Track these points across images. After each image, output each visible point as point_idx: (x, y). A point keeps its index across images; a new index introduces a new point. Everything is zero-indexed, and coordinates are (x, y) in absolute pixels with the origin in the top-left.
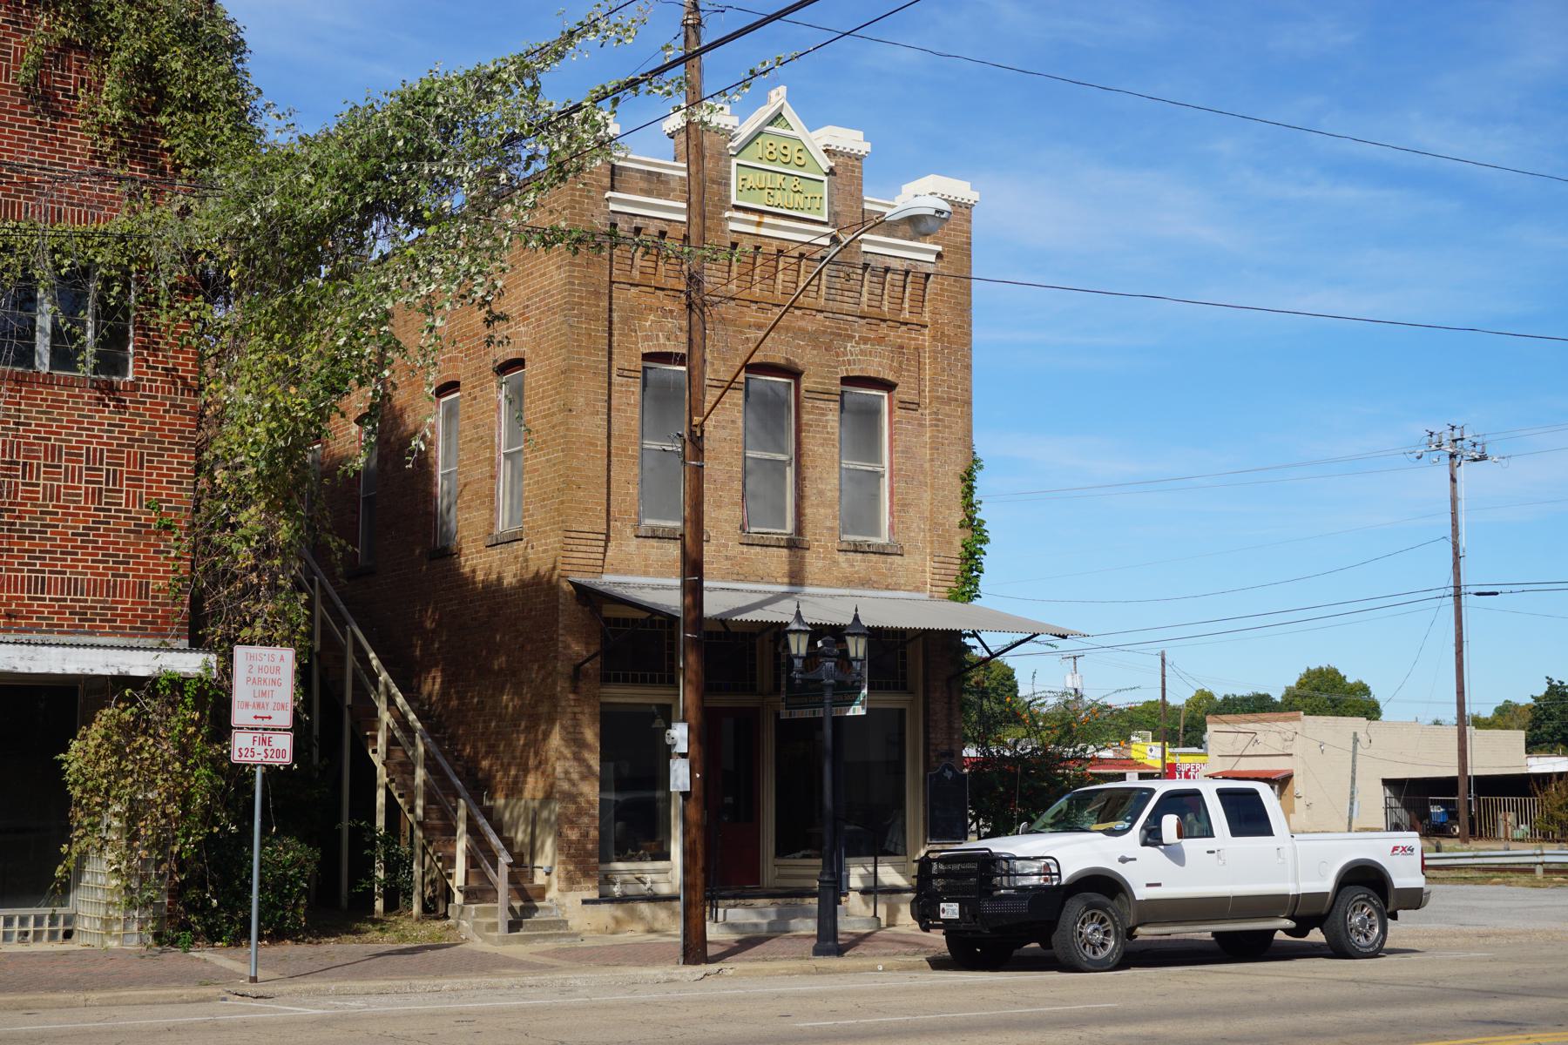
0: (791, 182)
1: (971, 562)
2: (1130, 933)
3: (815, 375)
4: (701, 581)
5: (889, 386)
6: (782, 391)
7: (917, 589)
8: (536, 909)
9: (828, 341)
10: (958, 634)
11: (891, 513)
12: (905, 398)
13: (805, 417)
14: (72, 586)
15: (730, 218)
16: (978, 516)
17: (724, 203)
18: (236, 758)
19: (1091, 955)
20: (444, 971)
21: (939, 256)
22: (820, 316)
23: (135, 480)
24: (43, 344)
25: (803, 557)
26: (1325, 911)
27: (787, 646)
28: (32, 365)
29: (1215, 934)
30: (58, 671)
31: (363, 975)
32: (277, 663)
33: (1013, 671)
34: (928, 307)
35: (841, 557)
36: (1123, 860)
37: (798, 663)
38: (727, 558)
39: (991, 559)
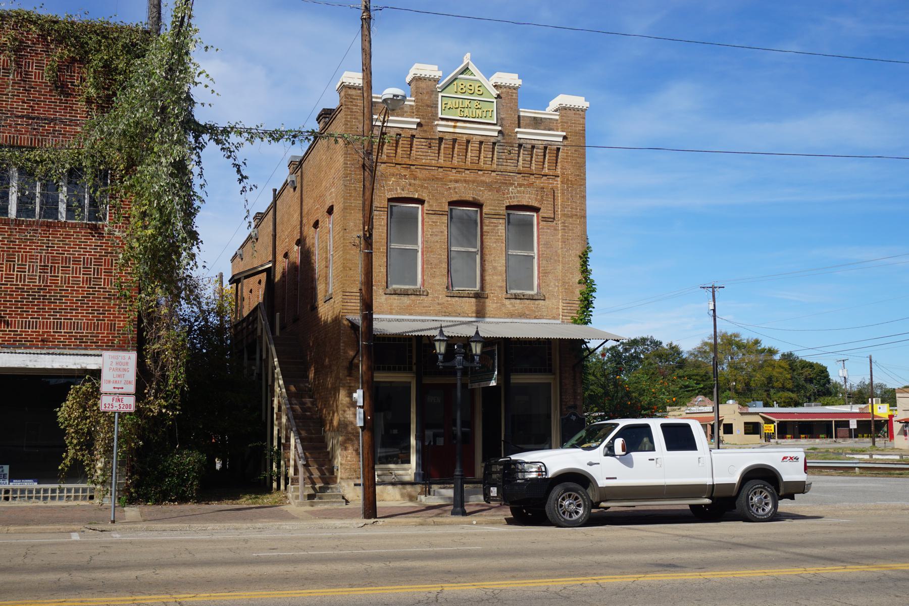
0: (474, 103)
1: (587, 303)
2: (596, 505)
3: (491, 205)
4: (372, 314)
5: (421, 202)
6: (473, 214)
7: (554, 318)
8: (328, 488)
9: (497, 188)
10: (582, 342)
11: (539, 278)
12: (545, 215)
13: (485, 228)
14: (75, 326)
15: (437, 125)
16: (591, 277)
17: (434, 116)
18: (103, 409)
19: (568, 518)
20: (272, 517)
21: (565, 138)
22: (494, 174)
23: (109, 272)
24: (62, 207)
25: (484, 303)
26: (734, 494)
27: (471, 350)
28: (57, 218)
29: (691, 506)
30: (50, 367)
31: (207, 520)
32: (127, 360)
33: (826, 368)
34: (559, 167)
35: (507, 302)
36: (591, 464)
37: (477, 358)
38: (439, 304)
39: (598, 303)
